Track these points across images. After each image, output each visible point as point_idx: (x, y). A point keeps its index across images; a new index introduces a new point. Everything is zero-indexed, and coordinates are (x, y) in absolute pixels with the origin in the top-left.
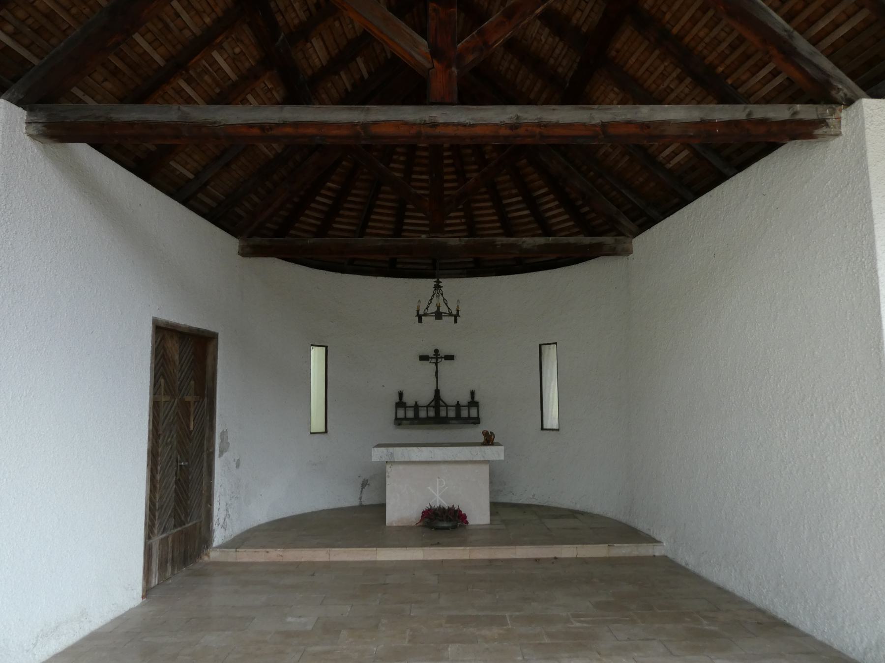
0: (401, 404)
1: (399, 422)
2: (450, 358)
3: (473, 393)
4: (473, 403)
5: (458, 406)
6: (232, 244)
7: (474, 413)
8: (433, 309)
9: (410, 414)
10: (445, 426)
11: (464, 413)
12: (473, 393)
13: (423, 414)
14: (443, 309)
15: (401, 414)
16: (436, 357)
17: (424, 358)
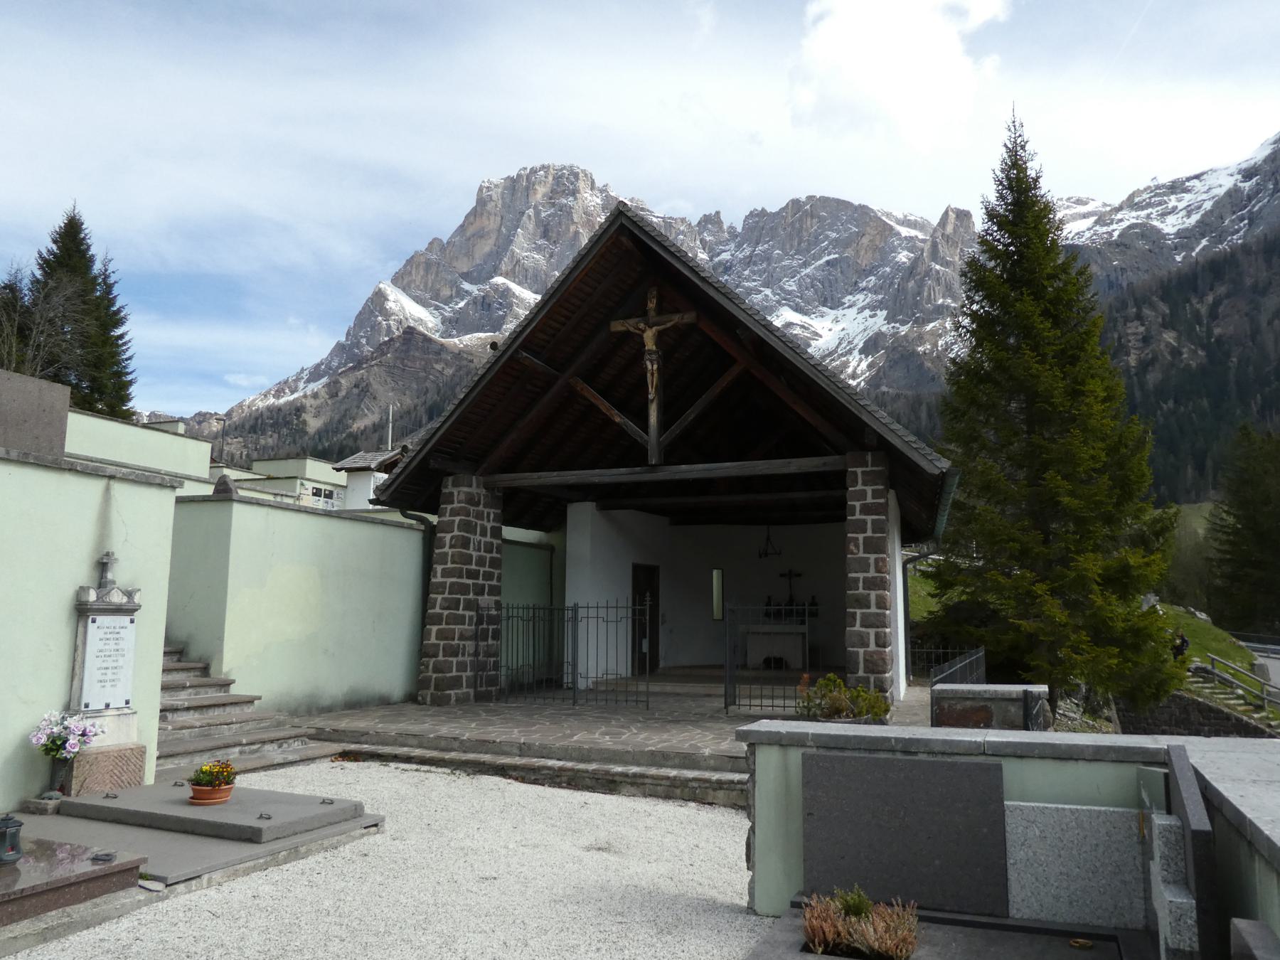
2: (799, 575)
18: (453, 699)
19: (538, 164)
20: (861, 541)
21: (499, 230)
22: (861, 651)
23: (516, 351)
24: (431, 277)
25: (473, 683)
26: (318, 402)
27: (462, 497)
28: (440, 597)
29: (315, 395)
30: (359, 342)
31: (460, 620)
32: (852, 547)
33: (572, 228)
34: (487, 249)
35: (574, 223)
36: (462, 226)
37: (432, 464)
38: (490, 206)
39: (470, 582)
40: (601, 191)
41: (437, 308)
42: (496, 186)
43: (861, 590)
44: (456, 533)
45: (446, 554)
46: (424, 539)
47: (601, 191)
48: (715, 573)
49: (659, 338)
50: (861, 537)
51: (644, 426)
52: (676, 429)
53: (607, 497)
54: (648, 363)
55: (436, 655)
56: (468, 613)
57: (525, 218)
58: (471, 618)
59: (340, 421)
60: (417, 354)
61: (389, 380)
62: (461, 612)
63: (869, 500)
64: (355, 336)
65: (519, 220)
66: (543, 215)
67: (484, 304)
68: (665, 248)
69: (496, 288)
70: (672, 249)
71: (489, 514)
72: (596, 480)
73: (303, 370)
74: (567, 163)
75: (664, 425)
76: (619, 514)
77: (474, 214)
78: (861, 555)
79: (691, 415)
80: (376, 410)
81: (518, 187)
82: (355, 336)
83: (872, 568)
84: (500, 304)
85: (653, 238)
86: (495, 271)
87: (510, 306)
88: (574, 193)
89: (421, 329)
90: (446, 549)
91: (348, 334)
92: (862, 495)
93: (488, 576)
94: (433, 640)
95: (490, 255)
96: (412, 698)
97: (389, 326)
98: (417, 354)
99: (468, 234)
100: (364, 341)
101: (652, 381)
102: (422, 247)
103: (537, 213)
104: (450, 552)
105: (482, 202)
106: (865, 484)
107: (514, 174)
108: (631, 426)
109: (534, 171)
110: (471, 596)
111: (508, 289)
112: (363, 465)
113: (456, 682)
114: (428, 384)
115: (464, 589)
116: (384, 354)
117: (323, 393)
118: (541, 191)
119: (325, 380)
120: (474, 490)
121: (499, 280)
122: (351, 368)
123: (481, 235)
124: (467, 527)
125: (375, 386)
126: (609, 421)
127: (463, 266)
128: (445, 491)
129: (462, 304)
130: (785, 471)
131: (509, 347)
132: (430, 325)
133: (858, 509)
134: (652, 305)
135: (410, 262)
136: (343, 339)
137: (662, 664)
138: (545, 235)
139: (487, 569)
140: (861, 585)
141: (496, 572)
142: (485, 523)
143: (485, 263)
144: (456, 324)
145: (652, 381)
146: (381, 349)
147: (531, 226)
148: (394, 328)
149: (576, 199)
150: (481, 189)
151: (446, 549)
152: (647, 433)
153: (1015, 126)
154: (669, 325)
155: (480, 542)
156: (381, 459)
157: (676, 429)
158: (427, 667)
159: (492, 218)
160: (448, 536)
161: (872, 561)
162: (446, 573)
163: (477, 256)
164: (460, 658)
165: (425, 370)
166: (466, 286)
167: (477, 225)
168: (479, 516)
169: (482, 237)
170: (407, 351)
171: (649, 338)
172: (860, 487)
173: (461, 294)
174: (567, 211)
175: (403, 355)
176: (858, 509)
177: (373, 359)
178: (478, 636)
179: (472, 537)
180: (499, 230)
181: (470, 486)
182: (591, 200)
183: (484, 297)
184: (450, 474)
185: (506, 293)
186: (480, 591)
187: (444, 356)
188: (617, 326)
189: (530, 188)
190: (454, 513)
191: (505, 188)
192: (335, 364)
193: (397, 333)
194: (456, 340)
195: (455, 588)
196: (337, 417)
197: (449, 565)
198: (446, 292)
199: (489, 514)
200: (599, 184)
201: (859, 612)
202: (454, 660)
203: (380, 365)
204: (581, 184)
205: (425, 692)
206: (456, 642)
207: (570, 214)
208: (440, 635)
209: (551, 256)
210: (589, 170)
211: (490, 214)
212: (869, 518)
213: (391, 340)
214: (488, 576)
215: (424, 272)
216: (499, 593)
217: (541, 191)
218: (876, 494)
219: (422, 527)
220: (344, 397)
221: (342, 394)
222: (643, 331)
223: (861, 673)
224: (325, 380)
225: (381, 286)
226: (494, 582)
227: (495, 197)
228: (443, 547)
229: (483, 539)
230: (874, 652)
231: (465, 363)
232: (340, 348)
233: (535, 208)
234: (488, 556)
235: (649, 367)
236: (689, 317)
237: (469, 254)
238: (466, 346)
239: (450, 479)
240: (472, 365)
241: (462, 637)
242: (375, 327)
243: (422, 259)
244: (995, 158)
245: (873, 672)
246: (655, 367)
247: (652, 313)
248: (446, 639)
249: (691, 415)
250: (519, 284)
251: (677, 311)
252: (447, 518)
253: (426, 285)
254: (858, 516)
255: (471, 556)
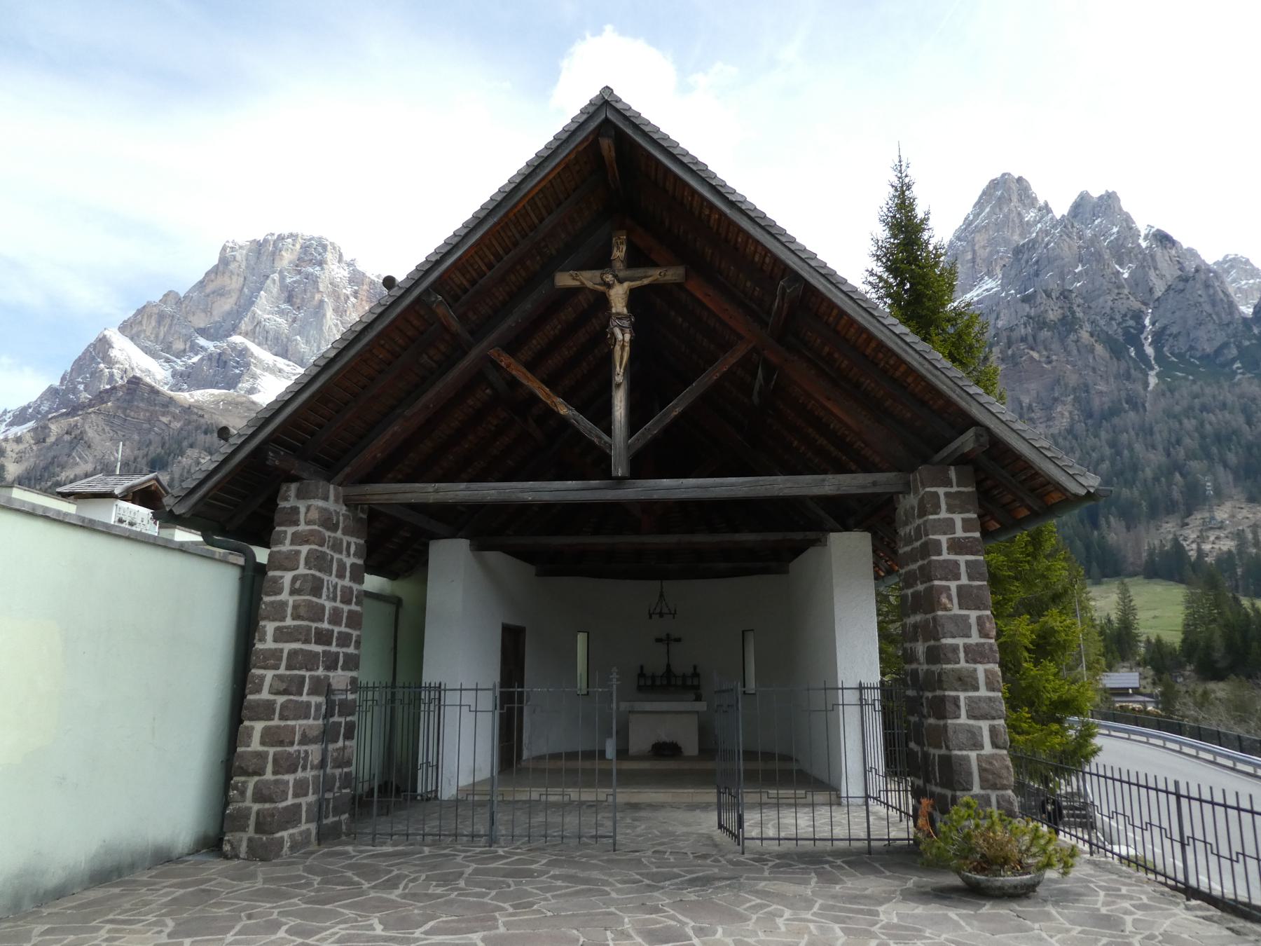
0: (642, 675)
1: (640, 688)
2: (678, 640)
3: (695, 668)
4: (696, 674)
5: (684, 677)
6: (530, 569)
7: (696, 683)
8: (658, 610)
9: (649, 682)
10: (947, 902)
11: (689, 682)
12: (695, 668)
13: (658, 683)
14: (665, 610)
15: (642, 683)
16: (667, 640)
17: (659, 640)
18: (287, 845)
19: (286, 232)
20: (954, 592)
21: (241, 290)
22: (973, 755)
23: (426, 291)
24: (163, 330)
25: (319, 812)
26: (21, 447)
27: (314, 515)
28: (269, 674)
29: (18, 440)
30: (75, 387)
31: (303, 711)
32: (944, 600)
33: (317, 297)
34: (227, 307)
35: (319, 291)
36: (201, 282)
37: (273, 459)
38: (233, 266)
39: (319, 649)
40: (349, 265)
41: (168, 361)
42: (241, 247)
43: (963, 664)
44: (302, 570)
45: (283, 604)
46: (242, 579)
47: (349, 265)
48: (581, 638)
49: (634, 298)
50: (953, 585)
51: (603, 417)
52: (652, 428)
53: (484, 528)
54: (617, 331)
55: (260, 772)
56: (315, 700)
57: (269, 282)
58: (318, 706)
59: (46, 468)
60: (141, 405)
61: (107, 429)
62: (304, 698)
63: (959, 533)
64: (72, 381)
65: (263, 283)
66: (288, 280)
67: (220, 361)
68: (674, 158)
69: (234, 347)
70: (685, 160)
71: (349, 544)
72: (529, 497)
73: (5, 412)
74: (316, 235)
75: (635, 422)
76: (494, 557)
77: (215, 271)
78: (956, 611)
79: (675, 409)
80: (91, 459)
81: (264, 251)
82: (72, 381)
83: (974, 631)
84: (238, 362)
85: (655, 142)
86: (234, 329)
87: (247, 365)
88: (321, 263)
89: (148, 380)
90: (284, 596)
91: (63, 379)
92: (948, 526)
93: (344, 640)
94: (255, 745)
95: (229, 313)
96: (212, 844)
97: (112, 375)
98: (141, 405)
99: (208, 290)
100: (81, 387)
101: (621, 357)
102: (156, 297)
103: (282, 278)
104: (291, 600)
105: (225, 261)
106: (950, 509)
107: (261, 238)
108: (584, 424)
109: (281, 238)
110: (321, 672)
111: (246, 349)
112: (99, 488)
113: (291, 817)
114: (152, 436)
115: (309, 661)
116: (103, 402)
117: (29, 438)
118: (287, 257)
119: (31, 424)
120: (331, 505)
121: (237, 339)
122: (62, 415)
123: (221, 293)
124: (319, 561)
125: (90, 433)
126: (551, 413)
127: (200, 321)
128: (282, 504)
129: (195, 359)
130: (816, 491)
131: (417, 283)
132: (159, 377)
133: (944, 546)
134: (619, 253)
135: (140, 312)
136: (56, 383)
137: (525, 755)
138: (289, 300)
139: (343, 629)
140: (962, 655)
141: (355, 633)
142: (345, 559)
143: (224, 321)
144: (188, 378)
145: (621, 357)
146: (101, 397)
147: (275, 290)
148: (117, 377)
149: (323, 269)
150: (224, 249)
151: (284, 596)
152: (608, 431)
153: (899, 168)
154: (646, 282)
155: (335, 587)
156: (128, 484)
157: (652, 428)
158: (243, 793)
159: (235, 278)
160: (288, 577)
161: (973, 620)
162: (281, 635)
163: (215, 313)
164: (300, 774)
165: (149, 421)
166: (202, 341)
167: (219, 282)
168: (336, 546)
169: (222, 295)
170: (130, 401)
171: (618, 298)
172: (944, 514)
173: (195, 349)
174: (314, 280)
175: (125, 405)
176: (944, 546)
177: (90, 406)
178: (328, 734)
179: (326, 578)
180: (241, 290)
181: (326, 498)
182: (338, 272)
183: (220, 354)
184: (295, 479)
185: (243, 353)
186: (332, 664)
187: (172, 409)
188: (565, 280)
189: (275, 254)
190: (299, 539)
191: (250, 250)
192: (45, 408)
193: (120, 382)
194: (186, 395)
195: (295, 660)
196: (42, 465)
197: (289, 622)
198: (179, 345)
199: (349, 544)
200: (347, 258)
201: (962, 696)
202: (290, 778)
203: (98, 413)
204: (329, 256)
205: (238, 835)
206: (296, 747)
207: (316, 282)
208: (270, 737)
209: (294, 321)
210: (337, 244)
211: (232, 273)
212: (962, 559)
213: (114, 388)
214: (344, 640)
215: (158, 322)
216: (356, 667)
217: (287, 257)
218: (967, 525)
219: (241, 561)
220: (54, 444)
221: (52, 439)
222: (610, 286)
223: (976, 789)
224: (31, 424)
225: (106, 333)
226: (351, 650)
227: (239, 258)
228: (280, 592)
229: (340, 583)
230: (993, 756)
231: (195, 417)
232: (52, 392)
233: (281, 272)
234: (346, 608)
235: (620, 336)
236: (672, 274)
237: (207, 311)
238: (197, 401)
239: (294, 487)
240: (202, 421)
241: (305, 740)
242: (97, 375)
243: (155, 310)
244: (881, 198)
245: (994, 787)
246: (627, 337)
247: (618, 265)
248: (281, 743)
249: (675, 409)
250: (259, 344)
251: (655, 265)
252: (286, 547)
253: (157, 337)
254: (945, 556)
255: (323, 607)
